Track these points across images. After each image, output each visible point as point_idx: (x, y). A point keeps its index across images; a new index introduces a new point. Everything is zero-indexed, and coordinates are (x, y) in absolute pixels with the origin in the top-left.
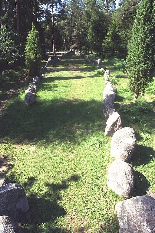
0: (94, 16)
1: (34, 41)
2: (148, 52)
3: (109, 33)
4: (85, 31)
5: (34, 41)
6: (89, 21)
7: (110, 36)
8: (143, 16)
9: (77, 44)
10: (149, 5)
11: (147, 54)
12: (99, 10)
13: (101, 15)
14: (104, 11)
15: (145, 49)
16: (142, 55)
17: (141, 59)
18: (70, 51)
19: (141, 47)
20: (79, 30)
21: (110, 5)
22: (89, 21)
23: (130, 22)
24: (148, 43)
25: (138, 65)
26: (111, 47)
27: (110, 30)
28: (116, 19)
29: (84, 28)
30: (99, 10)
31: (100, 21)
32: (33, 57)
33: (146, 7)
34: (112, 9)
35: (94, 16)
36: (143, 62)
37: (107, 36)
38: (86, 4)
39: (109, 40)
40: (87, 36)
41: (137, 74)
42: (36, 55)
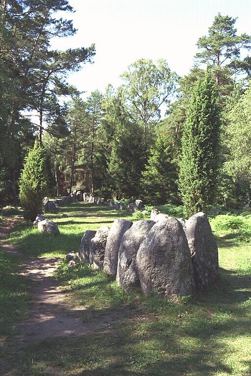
0: (120, 129)
1: (38, 163)
2: (202, 167)
3: (153, 160)
4: (103, 157)
5: (38, 163)
6: (110, 139)
7: (155, 165)
8: (190, 130)
9: (83, 184)
10: (194, 120)
11: (201, 168)
12: (130, 120)
13: (134, 128)
14: (140, 123)
15: (198, 164)
16: (195, 171)
17: (195, 175)
18: (73, 194)
19: (194, 162)
20: (89, 153)
21: (149, 112)
22: (110, 139)
23: (70, 53)
24: (200, 157)
25: (193, 182)
26: (157, 185)
27: (152, 153)
28: (162, 135)
29: (101, 152)
30: (130, 120)
31: (131, 139)
32: (35, 186)
33: (192, 121)
34: (154, 119)
35: (120, 129)
36: (197, 178)
37: (148, 164)
38: (104, 110)
39: (154, 171)
40: (107, 167)
41: (194, 194)
42: (39, 183)
